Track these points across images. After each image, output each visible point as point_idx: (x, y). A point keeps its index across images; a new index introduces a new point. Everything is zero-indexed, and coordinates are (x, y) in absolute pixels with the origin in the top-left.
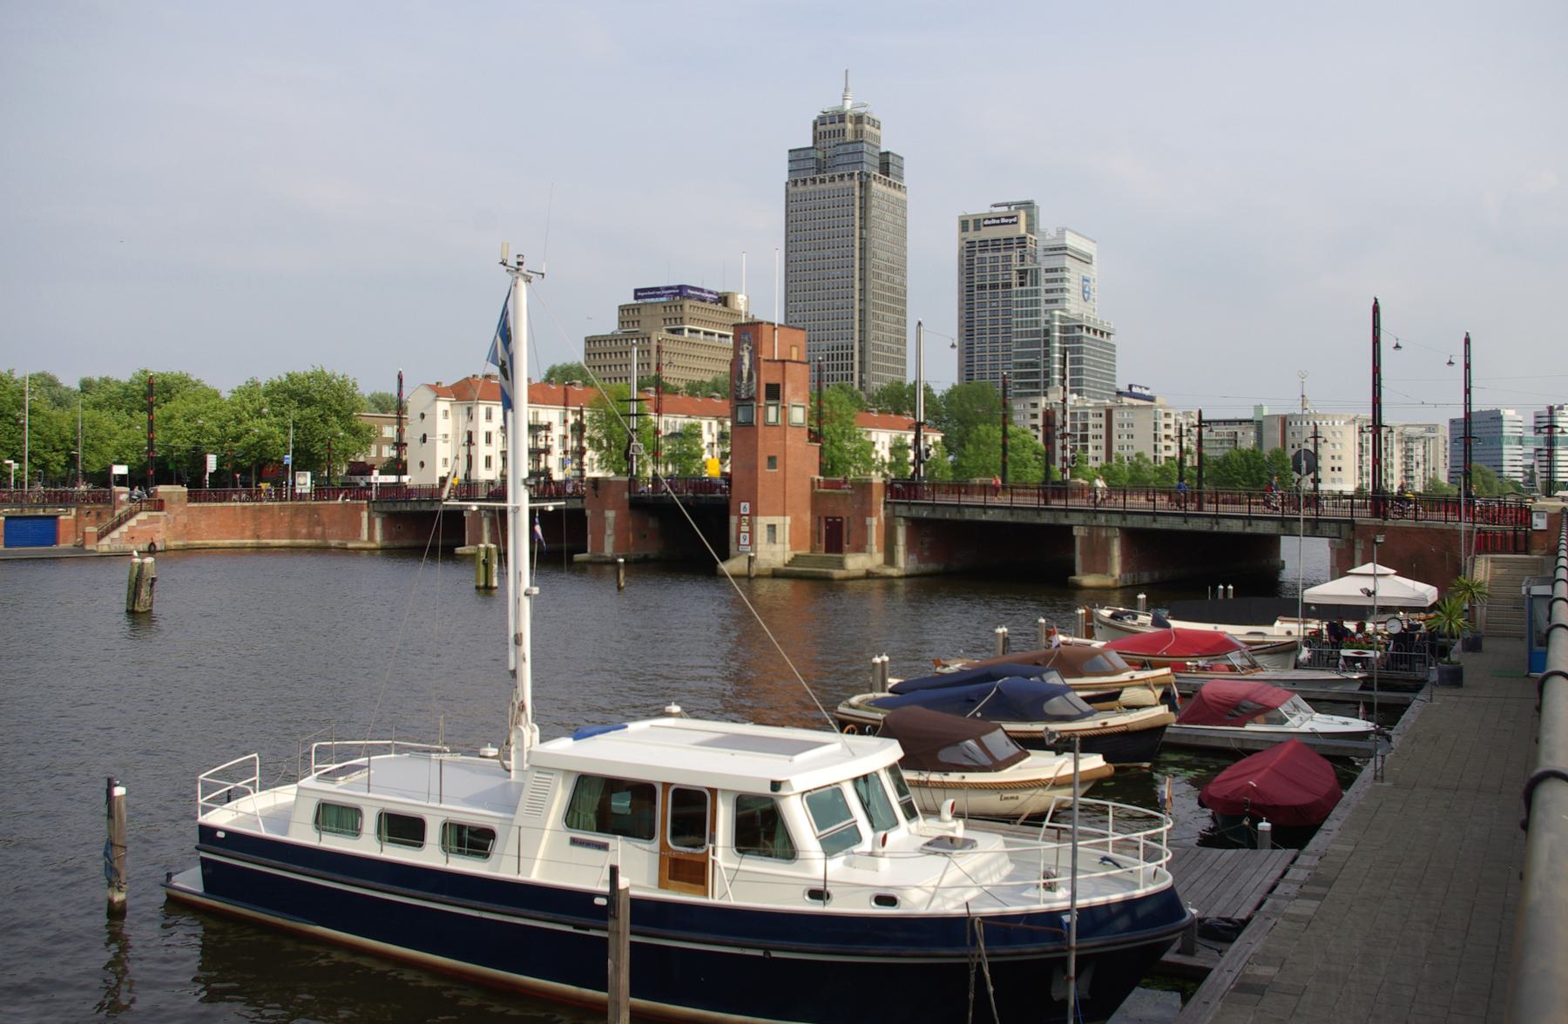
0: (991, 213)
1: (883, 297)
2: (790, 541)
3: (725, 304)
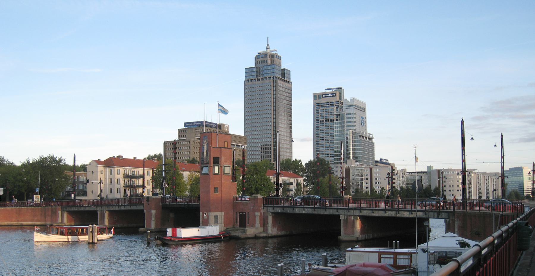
0: (325, 92)
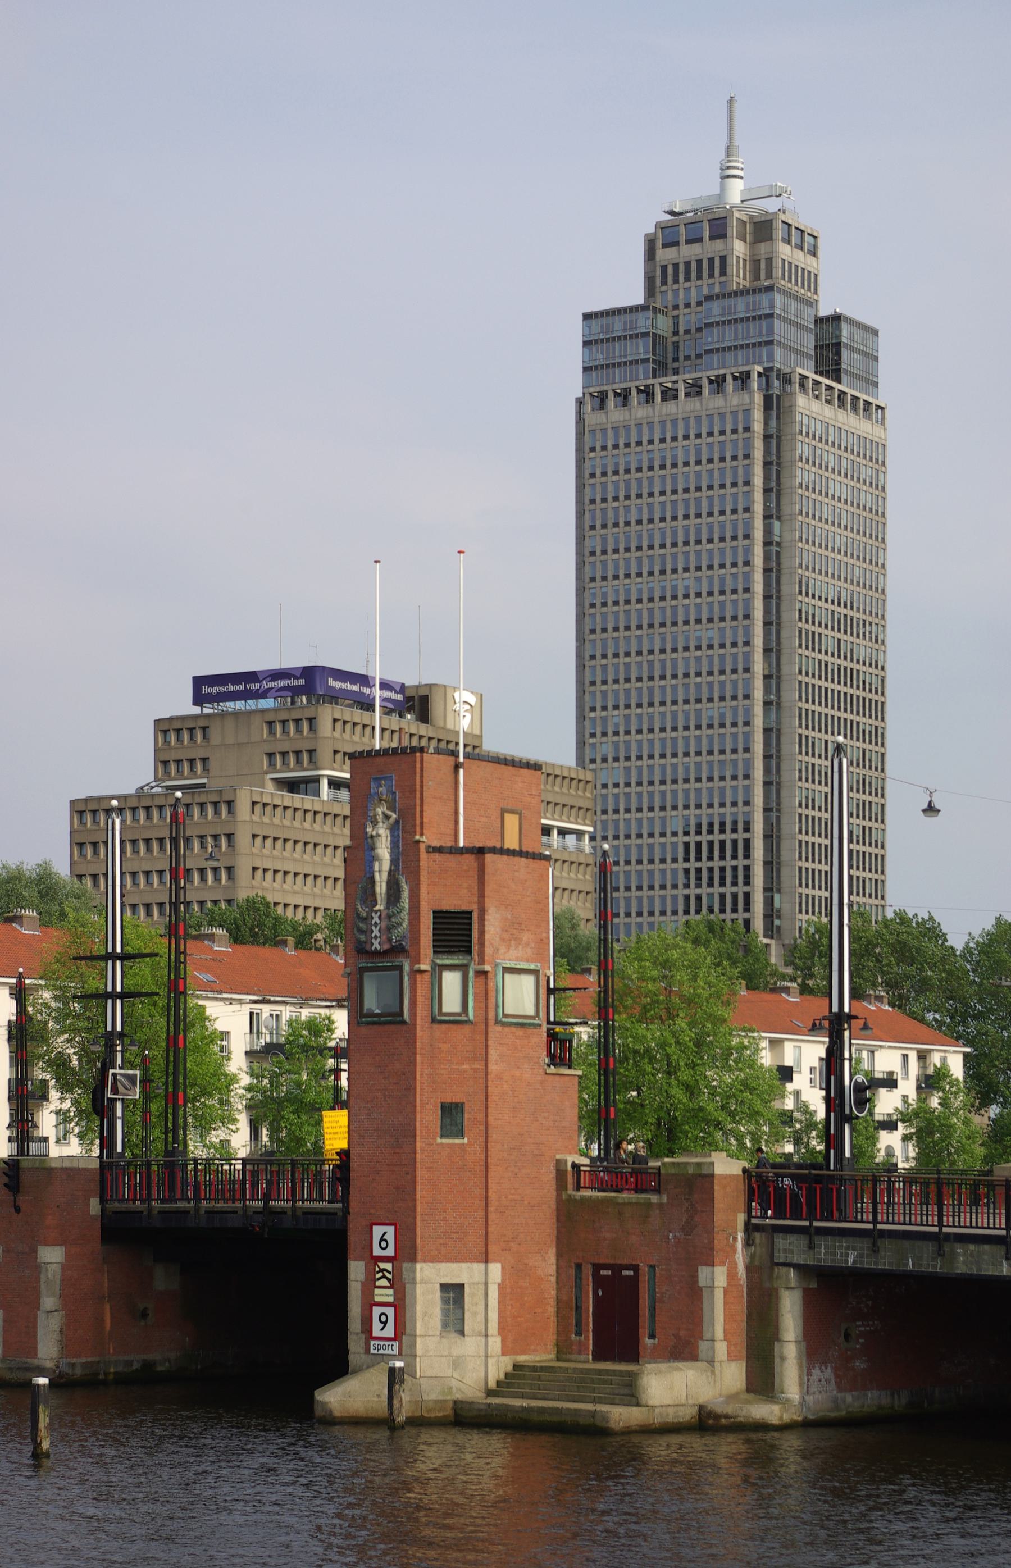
1: (825, 696)
2: (502, 1329)
3: (424, 717)
